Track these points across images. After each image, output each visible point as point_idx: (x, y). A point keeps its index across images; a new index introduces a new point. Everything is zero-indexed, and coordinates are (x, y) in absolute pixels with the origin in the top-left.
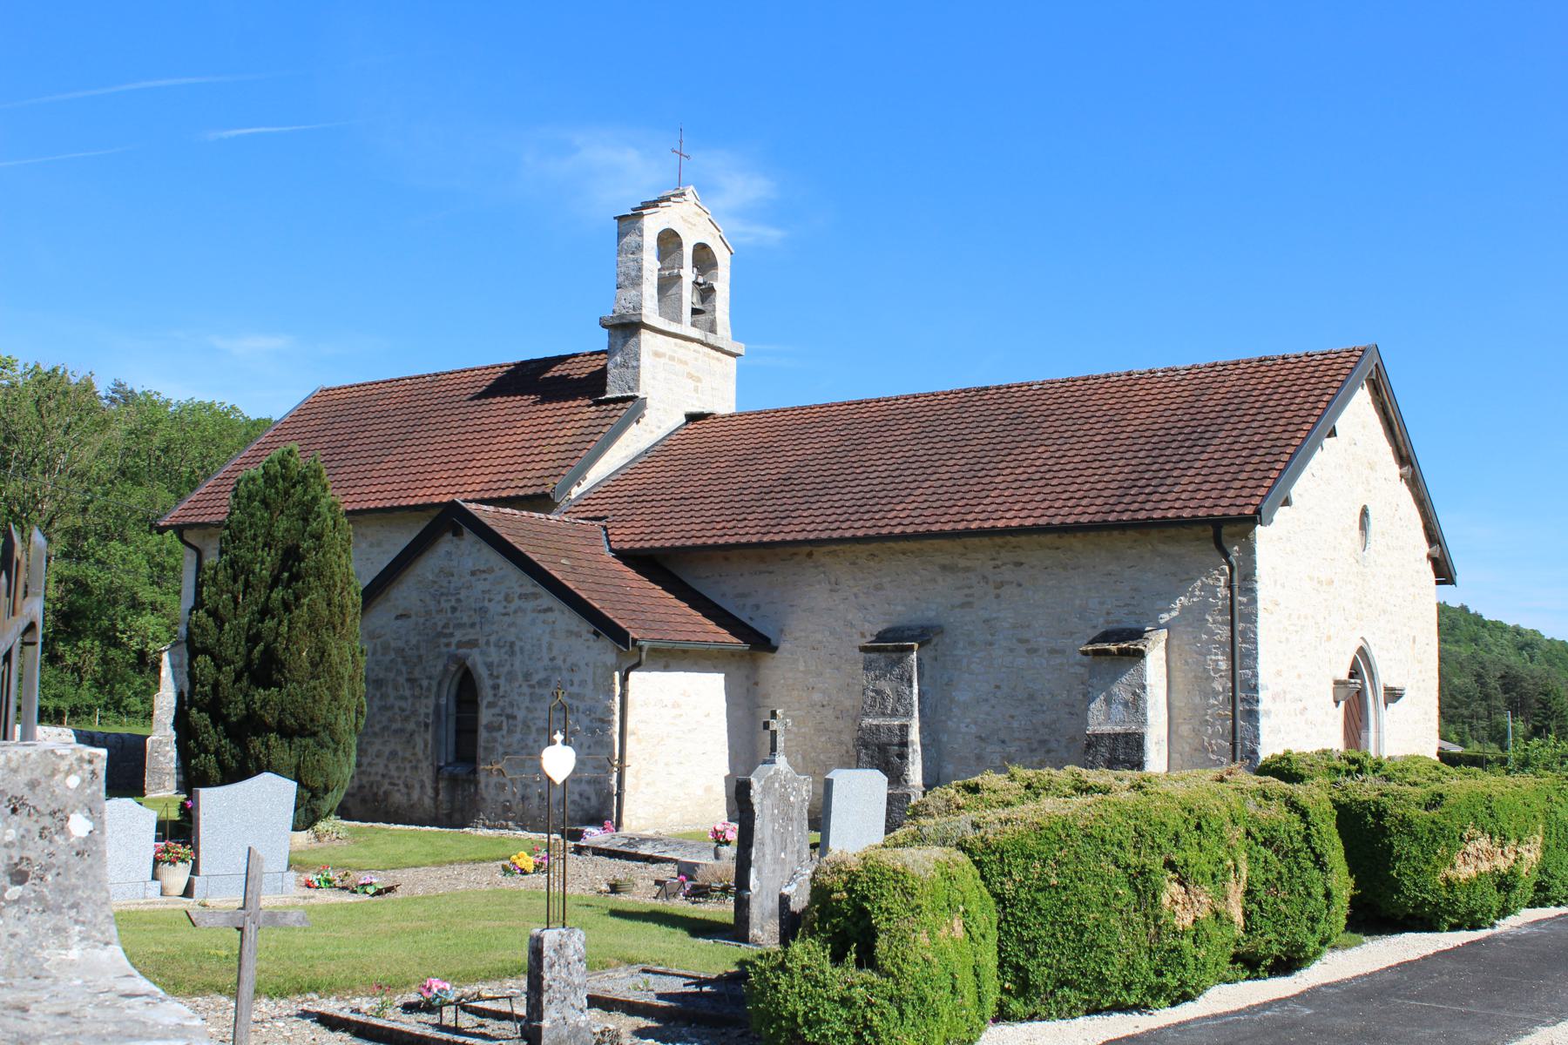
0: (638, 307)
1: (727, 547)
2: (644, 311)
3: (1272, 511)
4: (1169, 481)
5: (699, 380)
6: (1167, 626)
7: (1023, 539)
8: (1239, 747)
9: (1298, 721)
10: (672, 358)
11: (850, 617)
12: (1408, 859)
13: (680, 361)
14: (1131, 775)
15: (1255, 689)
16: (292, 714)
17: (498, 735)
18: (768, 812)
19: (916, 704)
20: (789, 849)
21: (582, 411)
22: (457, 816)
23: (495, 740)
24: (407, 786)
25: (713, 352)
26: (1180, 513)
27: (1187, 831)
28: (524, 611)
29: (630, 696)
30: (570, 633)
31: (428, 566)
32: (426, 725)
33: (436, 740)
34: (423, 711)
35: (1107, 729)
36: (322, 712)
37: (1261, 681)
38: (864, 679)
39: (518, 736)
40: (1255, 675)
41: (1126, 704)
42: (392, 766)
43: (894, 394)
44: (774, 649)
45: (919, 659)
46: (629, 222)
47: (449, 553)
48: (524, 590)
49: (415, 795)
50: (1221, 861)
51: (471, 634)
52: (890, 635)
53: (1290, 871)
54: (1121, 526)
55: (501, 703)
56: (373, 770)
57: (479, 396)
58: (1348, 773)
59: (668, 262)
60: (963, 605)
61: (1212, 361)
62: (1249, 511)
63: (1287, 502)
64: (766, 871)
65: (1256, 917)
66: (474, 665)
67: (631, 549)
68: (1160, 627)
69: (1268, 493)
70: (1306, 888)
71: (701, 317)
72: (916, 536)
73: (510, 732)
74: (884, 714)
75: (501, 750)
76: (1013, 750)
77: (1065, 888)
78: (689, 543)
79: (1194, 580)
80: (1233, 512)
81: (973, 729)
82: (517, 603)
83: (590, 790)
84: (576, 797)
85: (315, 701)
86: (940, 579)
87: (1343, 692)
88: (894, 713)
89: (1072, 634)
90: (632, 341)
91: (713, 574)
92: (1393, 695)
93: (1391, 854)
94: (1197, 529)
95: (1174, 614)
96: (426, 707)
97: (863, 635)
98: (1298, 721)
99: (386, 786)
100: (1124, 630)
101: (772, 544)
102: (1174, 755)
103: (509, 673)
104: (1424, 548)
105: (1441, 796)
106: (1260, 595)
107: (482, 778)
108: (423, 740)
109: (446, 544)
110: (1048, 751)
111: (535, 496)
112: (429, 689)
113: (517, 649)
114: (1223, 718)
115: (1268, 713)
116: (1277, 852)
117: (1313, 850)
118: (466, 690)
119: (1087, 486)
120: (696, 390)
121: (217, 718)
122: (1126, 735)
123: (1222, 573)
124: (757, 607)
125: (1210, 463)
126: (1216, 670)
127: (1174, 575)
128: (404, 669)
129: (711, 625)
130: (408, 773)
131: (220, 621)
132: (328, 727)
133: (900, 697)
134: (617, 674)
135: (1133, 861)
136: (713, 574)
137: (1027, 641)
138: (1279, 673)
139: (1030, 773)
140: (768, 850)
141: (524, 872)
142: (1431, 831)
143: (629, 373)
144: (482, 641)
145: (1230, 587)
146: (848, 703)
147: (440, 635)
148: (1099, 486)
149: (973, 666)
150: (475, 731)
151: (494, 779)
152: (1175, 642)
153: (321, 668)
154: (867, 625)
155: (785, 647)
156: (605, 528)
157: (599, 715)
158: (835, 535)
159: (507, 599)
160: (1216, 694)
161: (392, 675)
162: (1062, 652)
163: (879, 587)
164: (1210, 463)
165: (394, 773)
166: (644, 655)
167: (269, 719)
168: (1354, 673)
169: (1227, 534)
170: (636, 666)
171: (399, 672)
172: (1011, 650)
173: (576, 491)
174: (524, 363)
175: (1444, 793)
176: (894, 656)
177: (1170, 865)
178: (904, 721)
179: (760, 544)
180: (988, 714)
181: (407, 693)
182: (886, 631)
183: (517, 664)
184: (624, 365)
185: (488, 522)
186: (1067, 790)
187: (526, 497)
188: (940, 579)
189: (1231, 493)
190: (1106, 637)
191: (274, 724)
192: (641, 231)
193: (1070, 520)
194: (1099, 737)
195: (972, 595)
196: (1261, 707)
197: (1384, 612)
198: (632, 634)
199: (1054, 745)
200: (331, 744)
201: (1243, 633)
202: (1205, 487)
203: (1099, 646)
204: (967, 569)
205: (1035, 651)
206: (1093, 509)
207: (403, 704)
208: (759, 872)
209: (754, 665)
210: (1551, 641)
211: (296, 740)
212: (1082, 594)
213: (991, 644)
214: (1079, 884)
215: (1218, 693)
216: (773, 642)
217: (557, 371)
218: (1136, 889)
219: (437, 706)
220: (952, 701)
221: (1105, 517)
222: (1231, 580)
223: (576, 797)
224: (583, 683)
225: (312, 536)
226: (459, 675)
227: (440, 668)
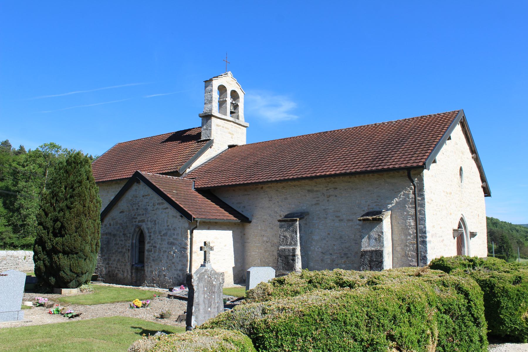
0: (211, 110)
1: (232, 186)
2: (213, 111)
3: (430, 165)
4: (390, 156)
7: (337, 179)
9: (440, 245)
10: (223, 127)
11: (276, 210)
12: (507, 308)
13: (226, 128)
14: (369, 274)
15: (425, 232)
16: (67, 246)
17: (151, 253)
18: (201, 290)
21: (193, 144)
22: (138, 282)
23: (150, 255)
24: (123, 271)
26: (394, 166)
27: (402, 313)
29: (194, 239)
30: (174, 216)
31: (129, 195)
32: (129, 250)
34: (128, 245)
35: (369, 249)
36: (78, 244)
37: (427, 229)
38: (280, 232)
39: (157, 254)
40: (425, 227)
41: (376, 239)
42: (118, 264)
43: (296, 136)
44: (250, 222)
46: (208, 82)
49: (125, 275)
50: (423, 332)
51: (143, 218)
52: (289, 216)
53: (460, 327)
54: (372, 172)
55: (152, 242)
56: (113, 266)
57: (163, 142)
58: (469, 266)
59: (222, 97)
60: (316, 204)
61: (404, 118)
62: (421, 164)
66: (144, 228)
67: (201, 188)
68: (388, 210)
69: (428, 158)
71: (234, 115)
72: (298, 179)
73: (155, 252)
74: (287, 245)
75: (152, 258)
76: (334, 257)
78: (220, 185)
80: (415, 165)
81: (320, 250)
82: (157, 206)
83: (180, 273)
84: (176, 276)
85: (75, 241)
87: (456, 234)
88: (291, 244)
89: (355, 213)
90: (209, 121)
91: (229, 197)
92: (473, 235)
94: (401, 172)
95: (393, 205)
96: (129, 244)
97: (280, 216)
98: (440, 245)
99: (117, 271)
100: (374, 212)
101: (248, 184)
102: (395, 258)
103: (154, 231)
104: (480, 184)
105: (520, 277)
106: (426, 197)
107: (146, 269)
108: (128, 255)
109: (135, 187)
110: (348, 258)
111: (174, 172)
112: (129, 237)
113: (157, 222)
116: (452, 317)
117: (473, 315)
119: (360, 159)
122: (376, 251)
123: (411, 189)
127: (393, 190)
128: (122, 230)
129: (227, 214)
130: (123, 267)
132: (82, 251)
133: (292, 238)
134: (189, 231)
136: (229, 197)
137: (339, 217)
138: (434, 227)
140: (201, 307)
141: (137, 307)
142: (517, 295)
143: (208, 132)
144: (146, 220)
145: (414, 193)
146: (276, 241)
148: (364, 159)
150: (144, 252)
151: (150, 269)
152: (394, 215)
153: (79, 230)
154: (282, 213)
155: (254, 221)
156: (194, 181)
157: (183, 246)
158: (269, 180)
159: (154, 205)
160: (410, 235)
161: (118, 233)
162: (352, 220)
163: (286, 199)
164: (405, 149)
165: (119, 267)
166: (198, 224)
167: (58, 248)
168: (460, 227)
169: (413, 173)
171: (121, 232)
172: (333, 220)
173: (188, 170)
175: (521, 275)
176: (290, 223)
177: (391, 337)
178: (294, 247)
179: (244, 184)
180: (325, 244)
181: (123, 239)
182: (288, 215)
184: (207, 129)
185: (148, 178)
186: (332, 284)
187: (171, 172)
189: (413, 158)
190: (368, 214)
191: (61, 250)
192: (212, 85)
193: (353, 171)
195: (319, 201)
196: (427, 239)
198: (193, 216)
199: (349, 255)
200: (84, 257)
201: (420, 211)
203: (365, 217)
204: (317, 191)
205: (342, 220)
206: (362, 167)
207: (121, 243)
208: (196, 318)
209: (244, 228)
211: (70, 255)
213: (326, 218)
216: (250, 219)
217: (187, 133)
219: (132, 243)
220: (312, 239)
221: (366, 169)
222: (415, 191)
223: (176, 276)
224: (178, 234)
225: (78, 182)
227: (133, 230)
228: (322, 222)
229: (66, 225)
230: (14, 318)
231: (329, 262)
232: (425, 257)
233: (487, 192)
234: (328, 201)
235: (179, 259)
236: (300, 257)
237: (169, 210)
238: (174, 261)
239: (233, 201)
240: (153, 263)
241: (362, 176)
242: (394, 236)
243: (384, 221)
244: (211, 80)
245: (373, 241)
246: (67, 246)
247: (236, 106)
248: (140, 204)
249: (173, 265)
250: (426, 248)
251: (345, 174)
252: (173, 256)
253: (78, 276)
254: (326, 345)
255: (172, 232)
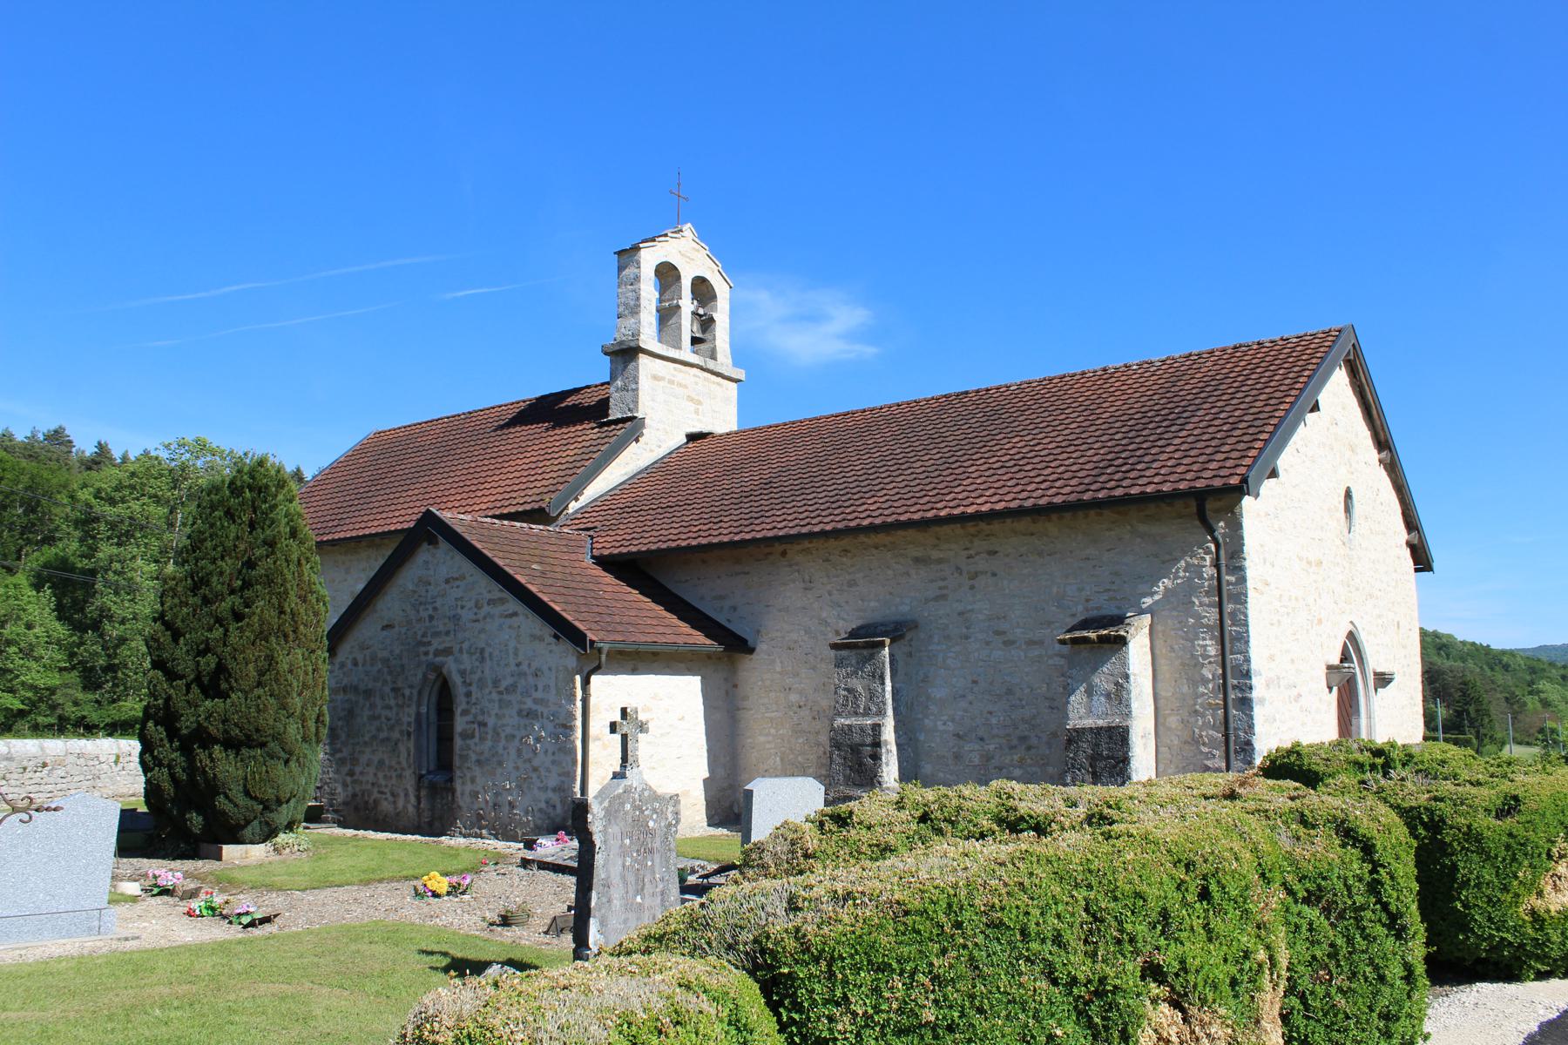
0: (636, 334)
2: (642, 337)
3: (1259, 483)
4: (1147, 459)
5: (700, 403)
6: (1150, 610)
7: (996, 526)
8: (1232, 738)
10: (671, 382)
11: (824, 615)
13: (680, 385)
14: (1091, 794)
15: (1248, 675)
16: (236, 725)
17: (470, 742)
19: (889, 702)
20: (648, 889)
21: (587, 432)
22: (437, 824)
24: (393, 795)
25: (714, 378)
27: (1185, 904)
28: (492, 617)
29: (593, 701)
30: (534, 637)
31: (408, 577)
32: (409, 734)
33: (418, 748)
34: (406, 719)
35: (1089, 723)
36: (267, 720)
37: (1254, 666)
38: (837, 676)
39: (489, 743)
40: (1247, 660)
41: (1108, 696)
42: (380, 775)
43: (879, 405)
44: (751, 651)
45: (891, 655)
46: (628, 255)
47: (426, 562)
48: (489, 596)
49: (401, 804)
50: (1247, 955)
51: (447, 642)
53: (1350, 941)
54: (1096, 504)
56: (364, 779)
57: (501, 427)
58: (1373, 767)
60: (936, 599)
61: (1187, 352)
62: (1234, 481)
63: (1274, 474)
64: (614, 922)
65: (1298, 1020)
67: (611, 555)
68: (1142, 612)
69: (1254, 463)
70: (1376, 968)
71: (702, 346)
72: (886, 528)
73: (482, 739)
74: (856, 714)
75: (474, 757)
76: (992, 747)
77: (950, 1029)
78: (664, 546)
79: (1177, 560)
80: (1217, 483)
81: (951, 727)
82: (486, 609)
84: (543, 805)
85: (259, 711)
86: (913, 572)
87: (1336, 678)
88: (867, 713)
89: (1049, 623)
90: (631, 366)
91: (692, 580)
92: (1383, 680)
93: (1454, 880)
94: (1179, 504)
95: (1157, 597)
96: (408, 716)
97: (837, 633)
98: (1292, 714)
99: (376, 795)
100: (1104, 617)
102: (1162, 749)
103: (480, 680)
104: (1403, 535)
105: (1516, 798)
106: (1250, 574)
107: (458, 785)
108: (407, 748)
109: (424, 554)
110: (1029, 748)
111: (533, 511)
112: (410, 698)
113: (487, 655)
114: (1214, 708)
115: (1262, 701)
116: (1326, 911)
117: (1385, 907)
118: (444, 698)
119: (1062, 469)
120: (697, 412)
121: (172, 733)
122: (1109, 729)
123: (1208, 552)
124: (734, 609)
125: (1190, 439)
126: (1205, 657)
127: (1156, 556)
129: (685, 628)
130: (394, 781)
131: (176, 635)
132: (277, 737)
133: (872, 695)
134: (578, 678)
135: (1083, 970)
136: (692, 580)
139: (930, 795)
140: (617, 894)
141: (435, 895)
142: (1508, 847)
144: (456, 648)
145: (1217, 565)
147: (421, 643)
148: (1074, 468)
149: (949, 661)
150: (451, 739)
151: (469, 787)
152: (1159, 628)
153: (267, 677)
154: (841, 623)
155: (762, 647)
157: (562, 721)
159: (478, 606)
160: (1205, 681)
162: (1040, 643)
163: (852, 584)
164: (1190, 439)
165: (383, 783)
166: (603, 657)
168: (1345, 657)
169: (1212, 507)
170: (597, 669)
171: (385, 682)
172: (988, 643)
173: (573, 506)
174: (543, 397)
175: (1520, 792)
176: (865, 652)
177: (1153, 972)
178: (876, 720)
179: (732, 544)
180: (966, 711)
182: (859, 628)
183: (487, 672)
184: (625, 389)
185: (459, 529)
186: (986, 823)
188: (913, 572)
189: (1213, 465)
190: (1085, 624)
192: (638, 263)
193: (1042, 502)
194: (1080, 732)
195: (945, 588)
196: (1255, 694)
197: (1371, 596)
198: (590, 636)
199: (1034, 741)
200: (282, 754)
201: (1233, 615)
202: (1185, 461)
203: (1077, 634)
204: (940, 561)
205: (1013, 642)
208: (603, 923)
209: (733, 668)
210: (1464, 643)
212: (1057, 582)
213: (967, 638)
214: (977, 1019)
215: (1208, 681)
217: (570, 401)
218: (1090, 1025)
219: (418, 714)
220: (928, 698)
222: (1218, 558)
223: (543, 805)
224: (546, 688)
225: (265, 542)
226: (438, 684)
227: (420, 676)
228: (957, 648)
229: (231, 665)
230: (90, 929)
231: (976, 761)
232: (1249, 743)
233: (1421, 559)
234: (972, 587)
235: (551, 758)
236: (894, 749)
237: (521, 618)
238: (536, 762)
239: (702, 591)
240: (477, 771)
241: (1068, 515)
242: (1159, 685)
243: (1131, 645)
244: (636, 249)
245: (1100, 702)
246: (236, 725)
247: (707, 323)
248: (438, 605)
249: (534, 776)
250: (1251, 717)
251: (1020, 513)
252: (534, 751)
253: (266, 808)
254: (972, 997)
255: (531, 679)
